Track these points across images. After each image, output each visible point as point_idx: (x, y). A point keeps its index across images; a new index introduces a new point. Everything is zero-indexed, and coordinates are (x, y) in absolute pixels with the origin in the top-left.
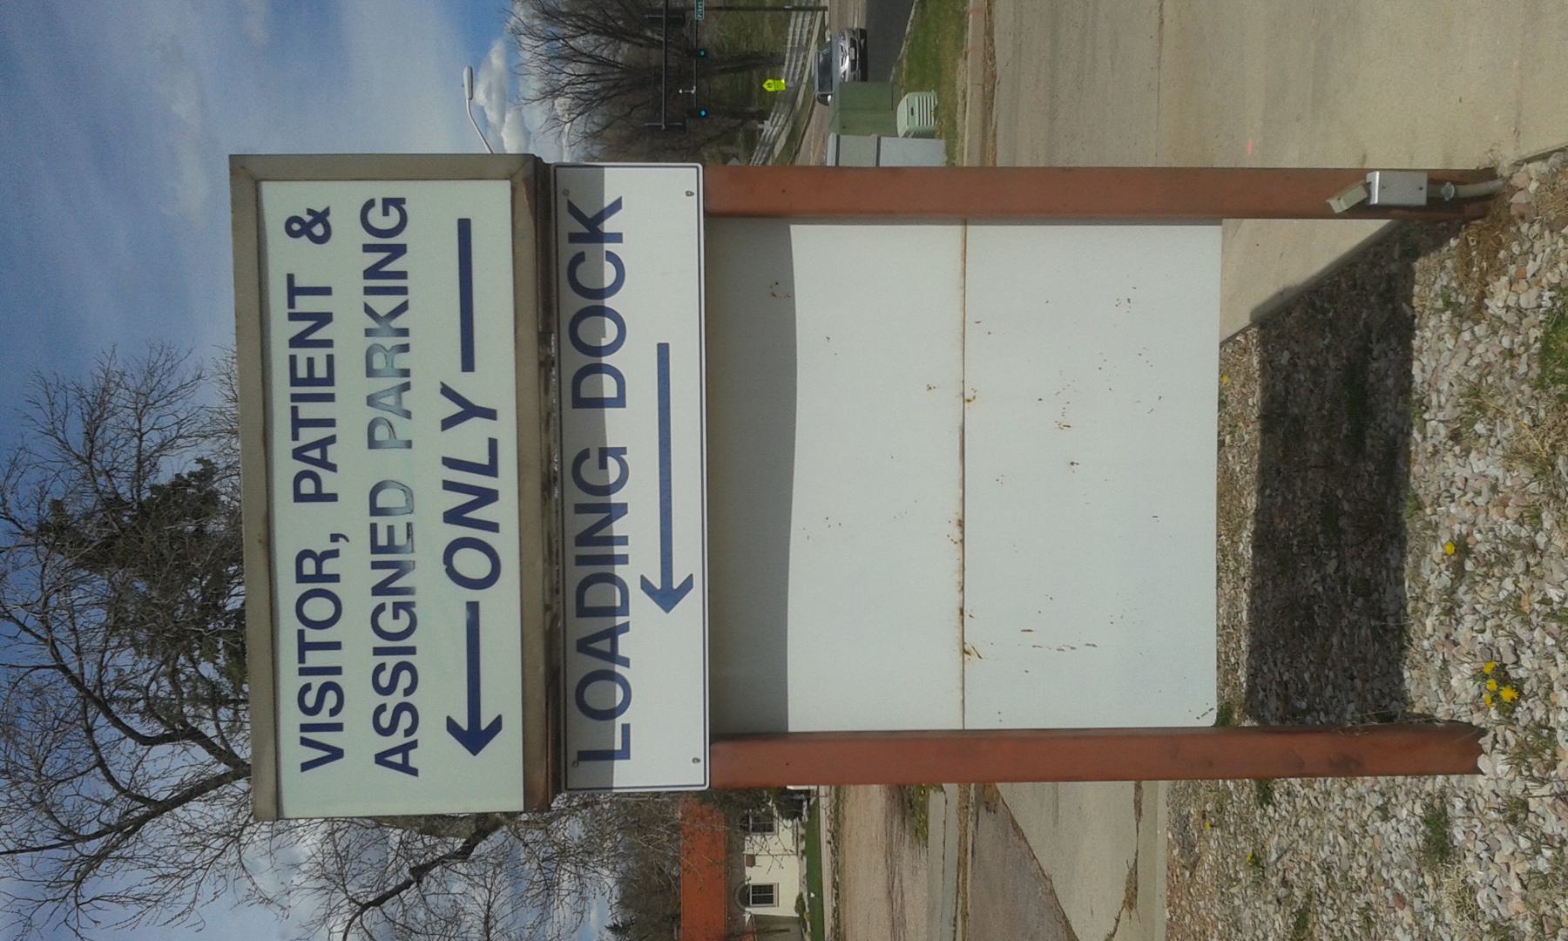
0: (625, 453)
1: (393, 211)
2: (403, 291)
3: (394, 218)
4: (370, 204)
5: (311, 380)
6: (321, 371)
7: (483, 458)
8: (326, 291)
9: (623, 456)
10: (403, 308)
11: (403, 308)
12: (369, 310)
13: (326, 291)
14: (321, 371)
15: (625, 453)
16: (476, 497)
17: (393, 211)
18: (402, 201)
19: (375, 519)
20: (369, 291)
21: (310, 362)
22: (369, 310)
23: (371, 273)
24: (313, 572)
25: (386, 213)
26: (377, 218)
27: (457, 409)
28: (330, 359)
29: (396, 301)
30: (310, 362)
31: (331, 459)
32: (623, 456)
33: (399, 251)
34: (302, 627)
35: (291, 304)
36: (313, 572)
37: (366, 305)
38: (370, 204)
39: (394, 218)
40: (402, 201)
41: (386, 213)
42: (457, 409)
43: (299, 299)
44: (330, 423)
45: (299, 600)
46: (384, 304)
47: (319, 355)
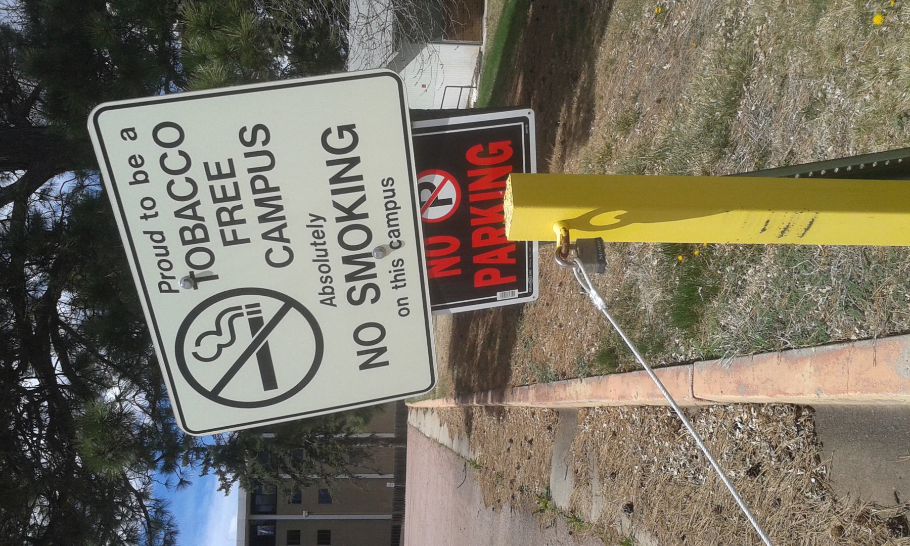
0: (355, 127)
1: (346, 134)
2: (361, 188)
3: (348, 138)
4: (328, 132)
5: (226, 198)
6: (231, 192)
8: (407, 298)
9: (354, 130)
10: (363, 199)
11: (363, 199)
12: (337, 205)
13: (407, 298)
14: (231, 192)
15: (355, 127)
16: (346, 215)
17: (346, 134)
18: (354, 126)
19: (212, 183)
20: (334, 192)
21: (223, 188)
22: (337, 205)
23: (335, 180)
24: (191, 238)
25: (341, 136)
26: (334, 141)
28: (236, 184)
29: (357, 195)
30: (223, 188)
31: (334, 303)
32: (354, 130)
33: (355, 161)
34: (192, 270)
36: (191, 238)
37: (333, 202)
38: (328, 132)
39: (348, 138)
40: (354, 126)
41: (341, 136)
43: (224, 172)
45: (186, 257)
46: (347, 200)
47: (228, 183)
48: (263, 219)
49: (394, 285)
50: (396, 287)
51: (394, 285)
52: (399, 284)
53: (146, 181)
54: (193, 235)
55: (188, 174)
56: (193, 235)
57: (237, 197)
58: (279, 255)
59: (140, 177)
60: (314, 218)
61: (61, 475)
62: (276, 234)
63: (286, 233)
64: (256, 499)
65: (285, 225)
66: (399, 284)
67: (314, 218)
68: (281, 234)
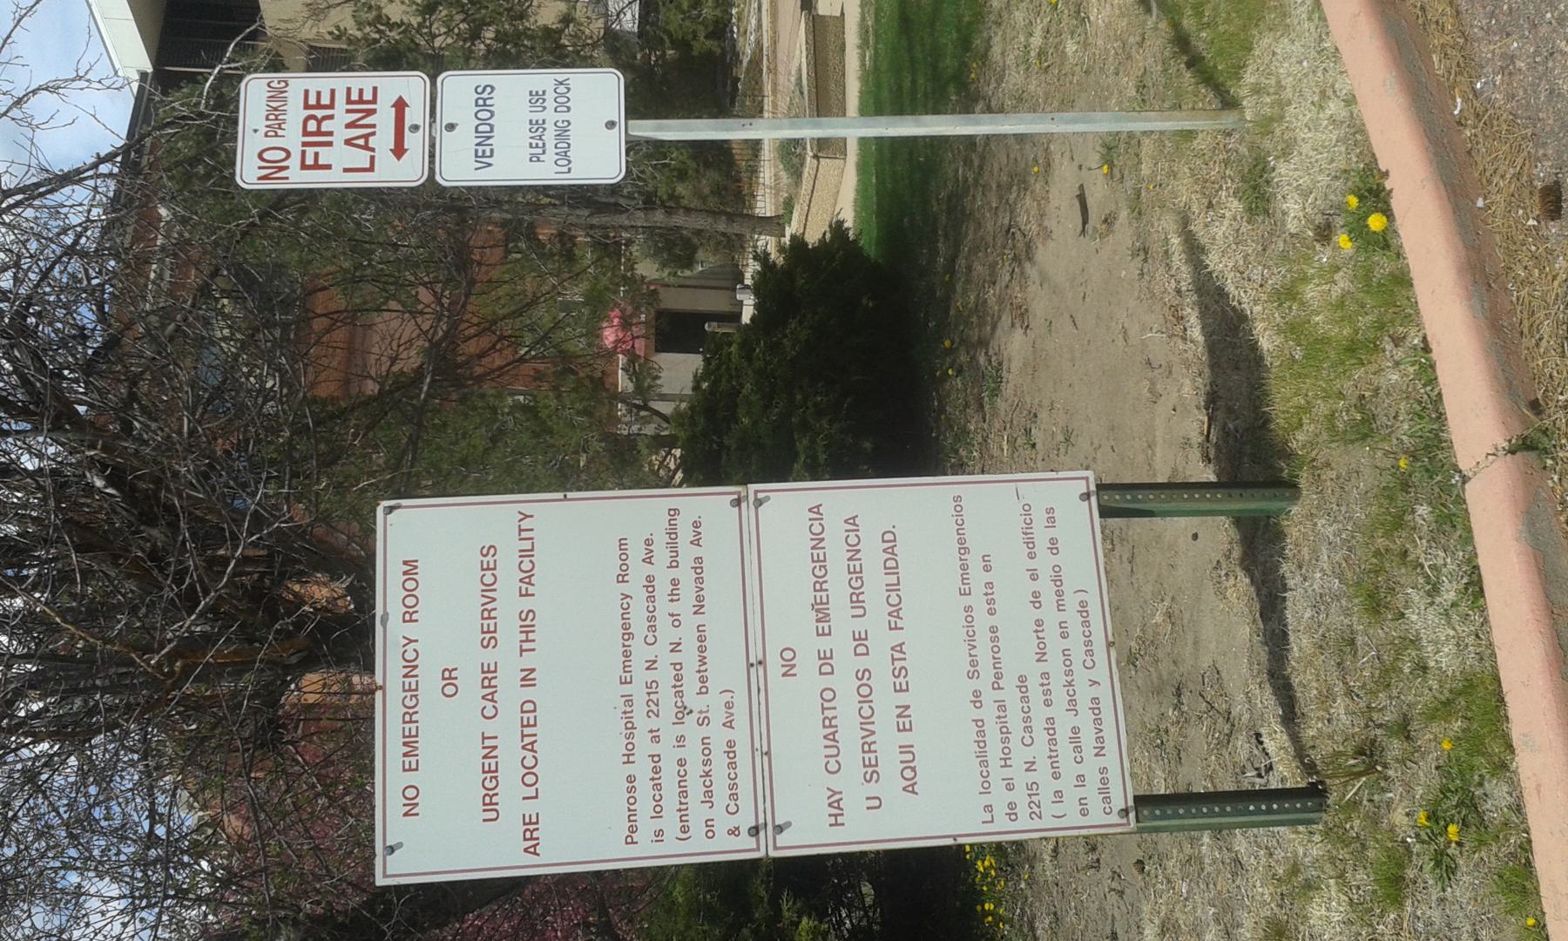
1: (859, 581)
3: (566, 124)
7: (530, 548)
17: (859, 581)
27: (522, 517)
35: (823, 713)
42: (522, 517)
44: (535, 735)
48: (350, 125)
49: (670, 598)
50: (672, 601)
51: (670, 598)
52: (675, 598)
53: (677, 567)
54: (319, 126)
55: (838, 758)
56: (319, 126)
57: (331, 106)
58: (833, 766)
59: (674, 564)
60: (867, 733)
61: (846, 897)
62: (361, 142)
63: (372, 142)
64: (1195, 424)
65: (373, 134)
66: (675, 598)
67: (867, 733)
68: (367, 142)
